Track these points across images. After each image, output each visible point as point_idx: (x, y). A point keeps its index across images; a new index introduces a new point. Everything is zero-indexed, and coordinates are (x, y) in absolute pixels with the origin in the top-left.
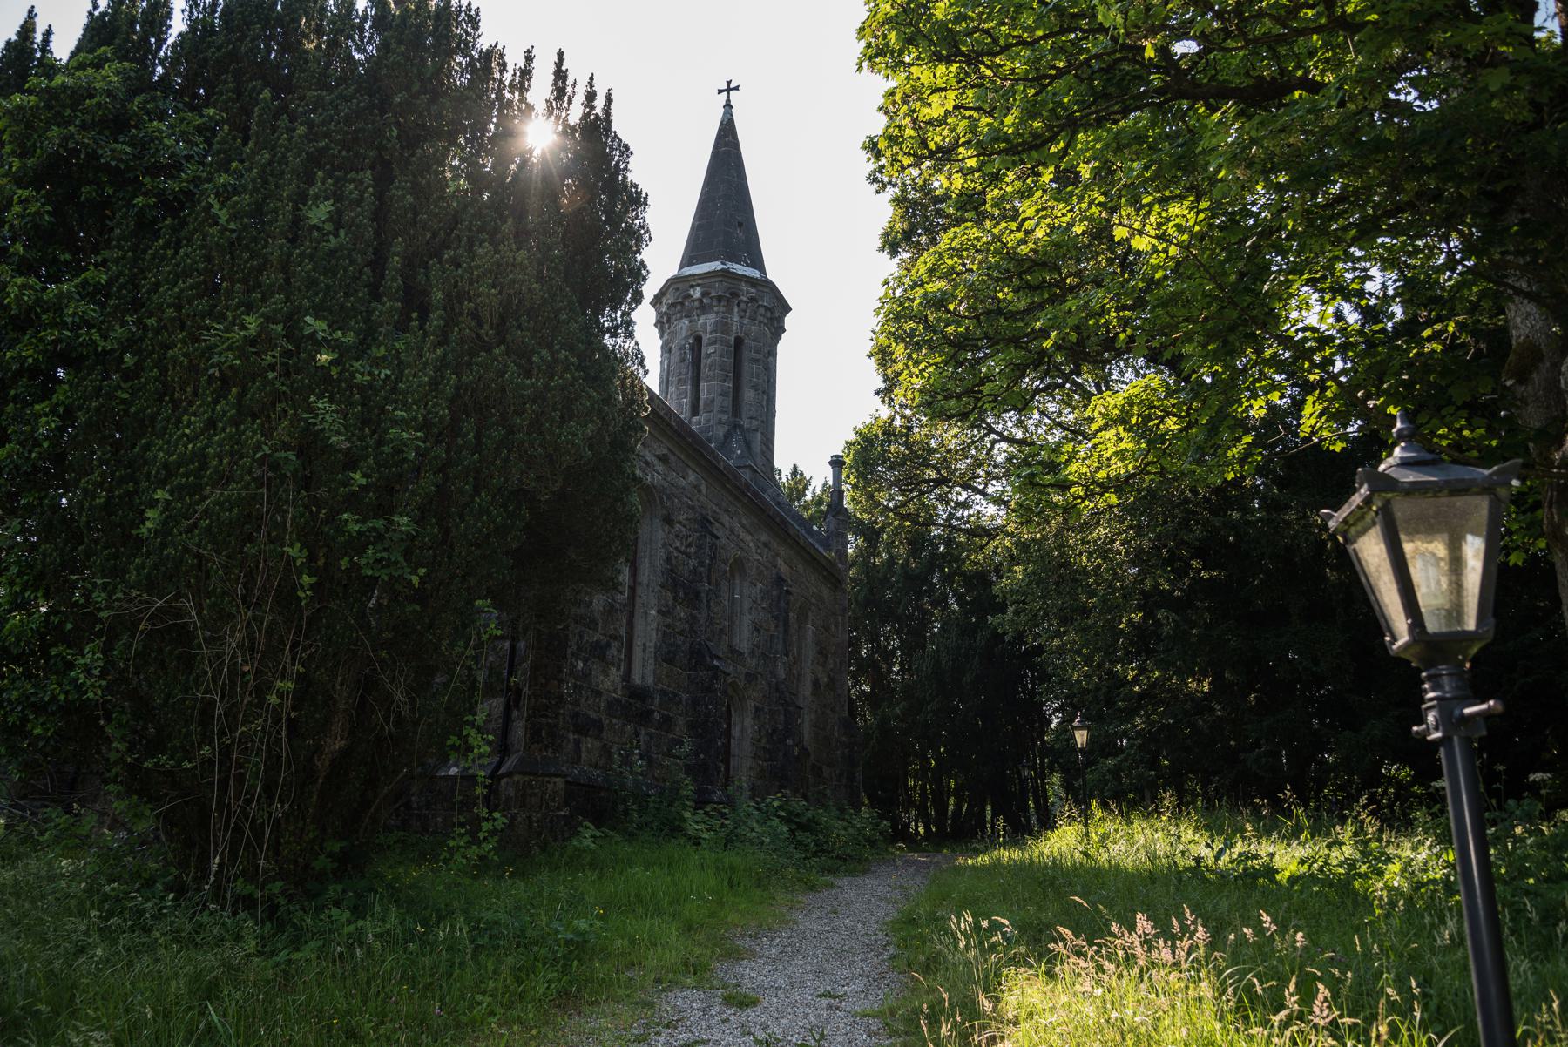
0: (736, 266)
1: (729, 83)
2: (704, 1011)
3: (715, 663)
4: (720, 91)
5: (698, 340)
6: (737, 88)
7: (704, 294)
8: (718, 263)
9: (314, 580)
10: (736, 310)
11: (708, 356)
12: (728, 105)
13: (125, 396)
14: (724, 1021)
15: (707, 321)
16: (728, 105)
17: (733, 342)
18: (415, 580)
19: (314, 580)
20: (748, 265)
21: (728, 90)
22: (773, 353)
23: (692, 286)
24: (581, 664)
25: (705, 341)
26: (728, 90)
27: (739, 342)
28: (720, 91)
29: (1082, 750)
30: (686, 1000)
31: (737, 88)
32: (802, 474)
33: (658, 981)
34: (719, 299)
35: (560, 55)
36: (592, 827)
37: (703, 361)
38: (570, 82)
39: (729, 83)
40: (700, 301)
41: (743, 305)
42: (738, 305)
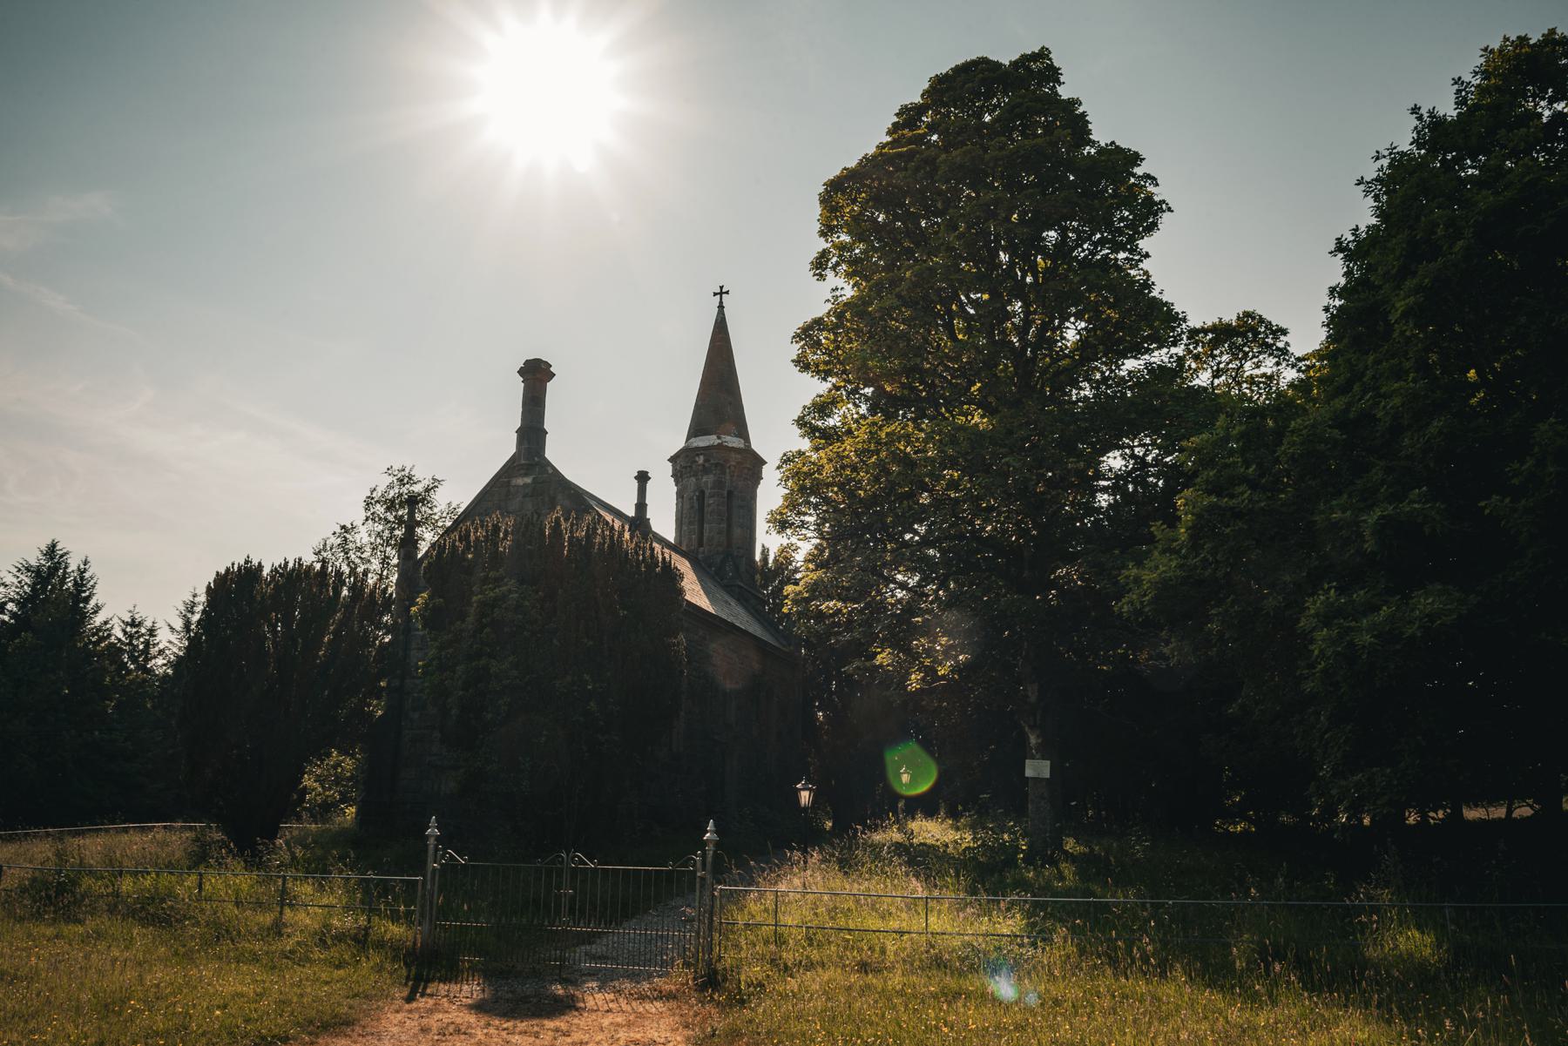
1: (721, 288)
4: (715, 294)
5: (702, 492)
6: (727, 293)
7: (705, 461)
8: (715, 437)
12: (721, 307)
16: (721, 307)
17: (726, 495)
20: (736, 436)
21: (721, 293)
22: (754, 497)
23: (698, 455)
26: (721, 293)
28: (715, 294)
31: (727, 293)
39: (721, 288)
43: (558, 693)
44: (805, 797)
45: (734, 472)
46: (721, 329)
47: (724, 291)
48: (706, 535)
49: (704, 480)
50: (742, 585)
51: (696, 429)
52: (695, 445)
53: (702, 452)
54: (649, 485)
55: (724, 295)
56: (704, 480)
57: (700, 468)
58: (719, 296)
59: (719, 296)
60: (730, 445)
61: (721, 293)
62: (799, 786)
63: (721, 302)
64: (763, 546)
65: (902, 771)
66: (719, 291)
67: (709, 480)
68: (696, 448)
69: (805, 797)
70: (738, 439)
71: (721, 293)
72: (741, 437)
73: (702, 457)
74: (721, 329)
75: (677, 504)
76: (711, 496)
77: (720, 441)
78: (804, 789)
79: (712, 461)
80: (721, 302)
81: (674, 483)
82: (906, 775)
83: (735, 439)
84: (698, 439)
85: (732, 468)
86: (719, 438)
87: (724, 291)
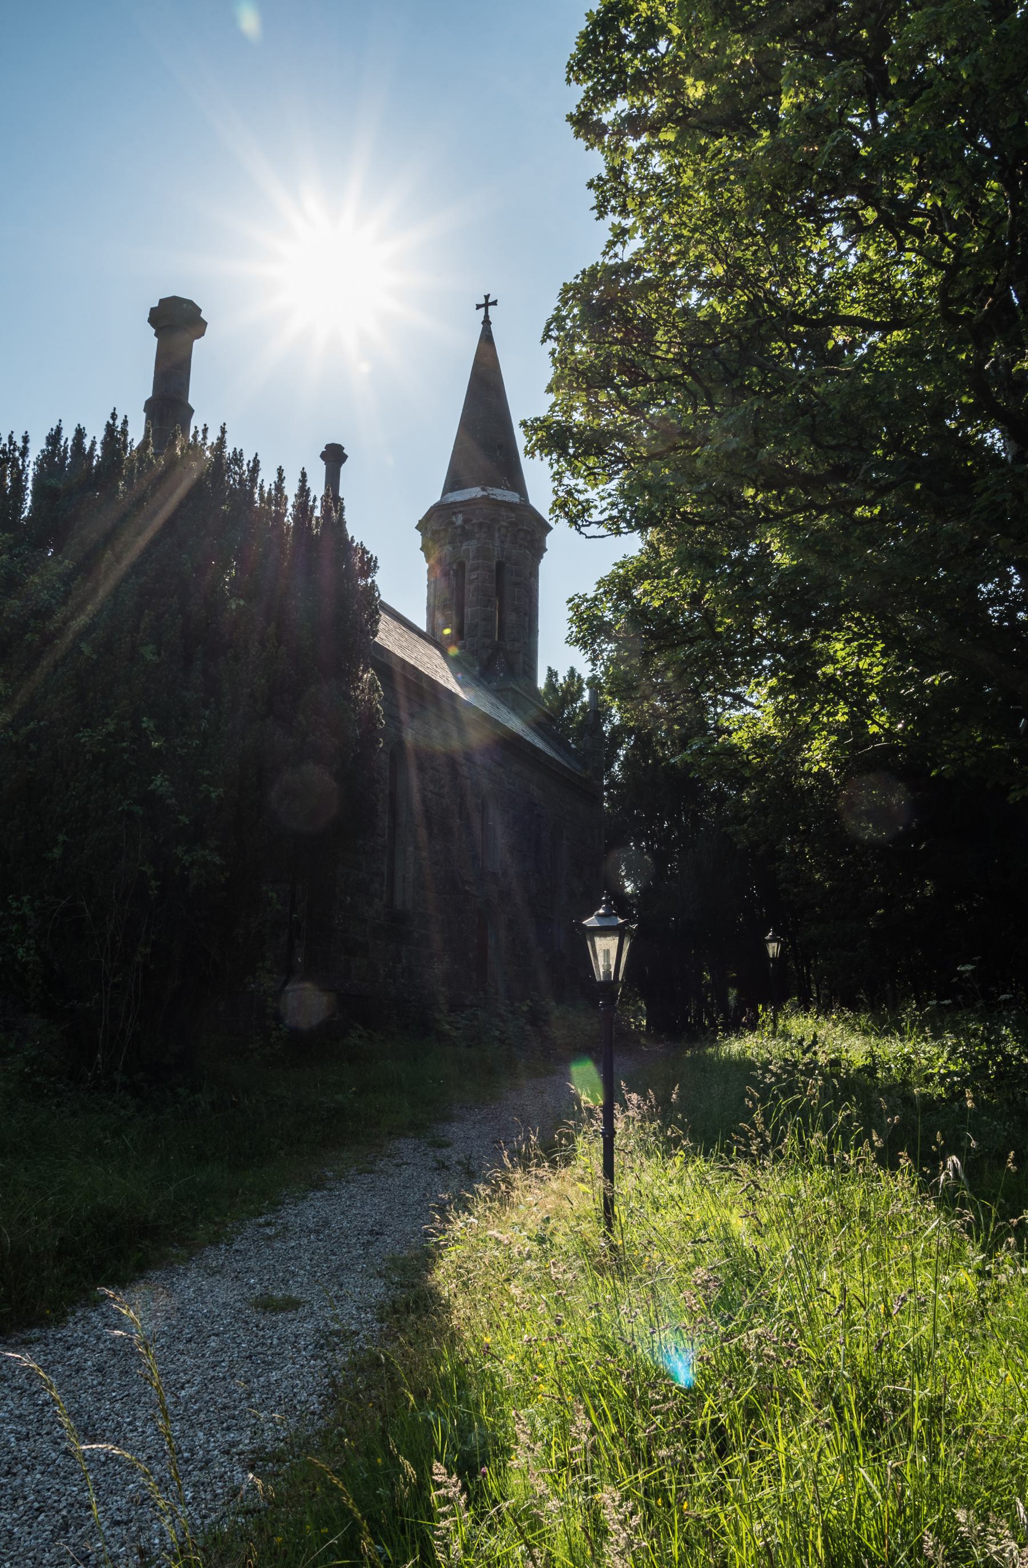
0: (497, 491)
1: (487, 297)
2: (415, 1150)
3: (467, 888)
4: (479, 307)
5: (462, 565)
6: (495, 303)
7: (465, 521)
8: (478, 489)
9: (159, 883)
10: (497, 535)
11: (471, 582)
12: (487, 322)
13: (31, 770)
14: (425, 1154)
15: (470, 547)
16: (487, 322)
17: (494, 567)
18: (223, 880)
19: (159, 883)
20: (508, 489)
21: (486, 305)
22: (534, 574)
23: (455, 514)
24: (349, 899)
25: (468, 567)
26: (486, 305)
27: (500, 566)
28: (479, 307)
29: (774, 959)
30: (406, 1146)
31: (495, 303)
32: (579, 676)
33: (390, 1133)
34: (480, 525)
35: (304, 475)
36: (361, 1028)
37: (467, 587)
38: (311, 498)
39: (487, 297)
40: (462, 527)
41: (503, 531)
42: (499, 530)
43: (88, 756)
44: (607, 953)
45: (506, 536)
46: (487, 338)
47: (490, 301)
48: (467, 621)
49: (464, 547)
50: (518, 689)
51: (453, 482)
52: (451, 500)
53: (461, 509)
54: (344, 469)
55: (490, 308)
56: (464, 547)
57: (459, 531)
58: (483, 309)
59: (483, 309)
60: (499, 498)
61: (487, 304)
62: (591, 922)
63: (487, 316)
64: (550, 669)
65: (767, 938)
66: (483, 302)
67: (470, 547)
68: (452, 503)
69: (607, 953)
70: (511, 493)
71: (487, 304)
72: (515, 491)
73: (460, 517)
74: (487, 338)
75: (428, 586)
76: (474, 569)
77: (485, 493)
78: (604, 931)
79: (474, 521)
80: (487, 316)
81: (424, 559)
82: (775, 944)
83: (506, 492)
84: (455, 493)
85: (503, 531)
86: (483, 490)
87: (490, 301)
